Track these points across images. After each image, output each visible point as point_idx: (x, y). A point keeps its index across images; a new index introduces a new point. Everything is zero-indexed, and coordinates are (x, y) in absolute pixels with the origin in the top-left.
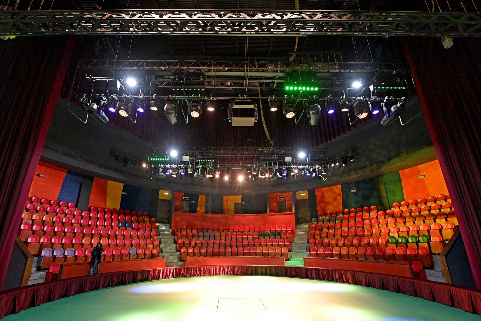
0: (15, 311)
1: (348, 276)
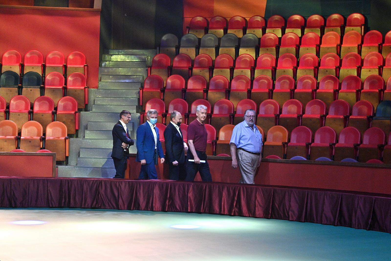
0: (186, 33)
1: (256, 198)
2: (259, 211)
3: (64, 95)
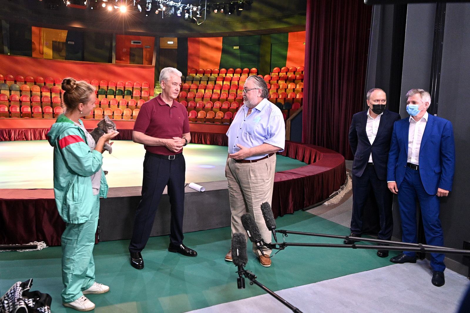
2: (208, 142)
3: (141, 99)
